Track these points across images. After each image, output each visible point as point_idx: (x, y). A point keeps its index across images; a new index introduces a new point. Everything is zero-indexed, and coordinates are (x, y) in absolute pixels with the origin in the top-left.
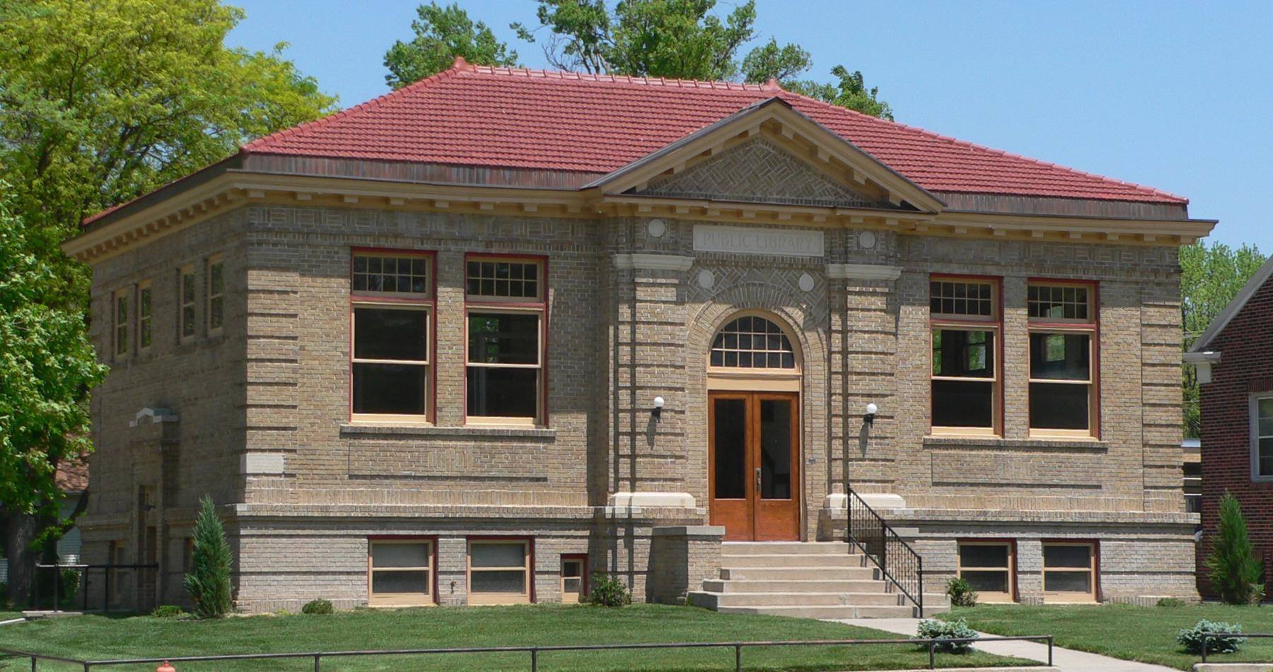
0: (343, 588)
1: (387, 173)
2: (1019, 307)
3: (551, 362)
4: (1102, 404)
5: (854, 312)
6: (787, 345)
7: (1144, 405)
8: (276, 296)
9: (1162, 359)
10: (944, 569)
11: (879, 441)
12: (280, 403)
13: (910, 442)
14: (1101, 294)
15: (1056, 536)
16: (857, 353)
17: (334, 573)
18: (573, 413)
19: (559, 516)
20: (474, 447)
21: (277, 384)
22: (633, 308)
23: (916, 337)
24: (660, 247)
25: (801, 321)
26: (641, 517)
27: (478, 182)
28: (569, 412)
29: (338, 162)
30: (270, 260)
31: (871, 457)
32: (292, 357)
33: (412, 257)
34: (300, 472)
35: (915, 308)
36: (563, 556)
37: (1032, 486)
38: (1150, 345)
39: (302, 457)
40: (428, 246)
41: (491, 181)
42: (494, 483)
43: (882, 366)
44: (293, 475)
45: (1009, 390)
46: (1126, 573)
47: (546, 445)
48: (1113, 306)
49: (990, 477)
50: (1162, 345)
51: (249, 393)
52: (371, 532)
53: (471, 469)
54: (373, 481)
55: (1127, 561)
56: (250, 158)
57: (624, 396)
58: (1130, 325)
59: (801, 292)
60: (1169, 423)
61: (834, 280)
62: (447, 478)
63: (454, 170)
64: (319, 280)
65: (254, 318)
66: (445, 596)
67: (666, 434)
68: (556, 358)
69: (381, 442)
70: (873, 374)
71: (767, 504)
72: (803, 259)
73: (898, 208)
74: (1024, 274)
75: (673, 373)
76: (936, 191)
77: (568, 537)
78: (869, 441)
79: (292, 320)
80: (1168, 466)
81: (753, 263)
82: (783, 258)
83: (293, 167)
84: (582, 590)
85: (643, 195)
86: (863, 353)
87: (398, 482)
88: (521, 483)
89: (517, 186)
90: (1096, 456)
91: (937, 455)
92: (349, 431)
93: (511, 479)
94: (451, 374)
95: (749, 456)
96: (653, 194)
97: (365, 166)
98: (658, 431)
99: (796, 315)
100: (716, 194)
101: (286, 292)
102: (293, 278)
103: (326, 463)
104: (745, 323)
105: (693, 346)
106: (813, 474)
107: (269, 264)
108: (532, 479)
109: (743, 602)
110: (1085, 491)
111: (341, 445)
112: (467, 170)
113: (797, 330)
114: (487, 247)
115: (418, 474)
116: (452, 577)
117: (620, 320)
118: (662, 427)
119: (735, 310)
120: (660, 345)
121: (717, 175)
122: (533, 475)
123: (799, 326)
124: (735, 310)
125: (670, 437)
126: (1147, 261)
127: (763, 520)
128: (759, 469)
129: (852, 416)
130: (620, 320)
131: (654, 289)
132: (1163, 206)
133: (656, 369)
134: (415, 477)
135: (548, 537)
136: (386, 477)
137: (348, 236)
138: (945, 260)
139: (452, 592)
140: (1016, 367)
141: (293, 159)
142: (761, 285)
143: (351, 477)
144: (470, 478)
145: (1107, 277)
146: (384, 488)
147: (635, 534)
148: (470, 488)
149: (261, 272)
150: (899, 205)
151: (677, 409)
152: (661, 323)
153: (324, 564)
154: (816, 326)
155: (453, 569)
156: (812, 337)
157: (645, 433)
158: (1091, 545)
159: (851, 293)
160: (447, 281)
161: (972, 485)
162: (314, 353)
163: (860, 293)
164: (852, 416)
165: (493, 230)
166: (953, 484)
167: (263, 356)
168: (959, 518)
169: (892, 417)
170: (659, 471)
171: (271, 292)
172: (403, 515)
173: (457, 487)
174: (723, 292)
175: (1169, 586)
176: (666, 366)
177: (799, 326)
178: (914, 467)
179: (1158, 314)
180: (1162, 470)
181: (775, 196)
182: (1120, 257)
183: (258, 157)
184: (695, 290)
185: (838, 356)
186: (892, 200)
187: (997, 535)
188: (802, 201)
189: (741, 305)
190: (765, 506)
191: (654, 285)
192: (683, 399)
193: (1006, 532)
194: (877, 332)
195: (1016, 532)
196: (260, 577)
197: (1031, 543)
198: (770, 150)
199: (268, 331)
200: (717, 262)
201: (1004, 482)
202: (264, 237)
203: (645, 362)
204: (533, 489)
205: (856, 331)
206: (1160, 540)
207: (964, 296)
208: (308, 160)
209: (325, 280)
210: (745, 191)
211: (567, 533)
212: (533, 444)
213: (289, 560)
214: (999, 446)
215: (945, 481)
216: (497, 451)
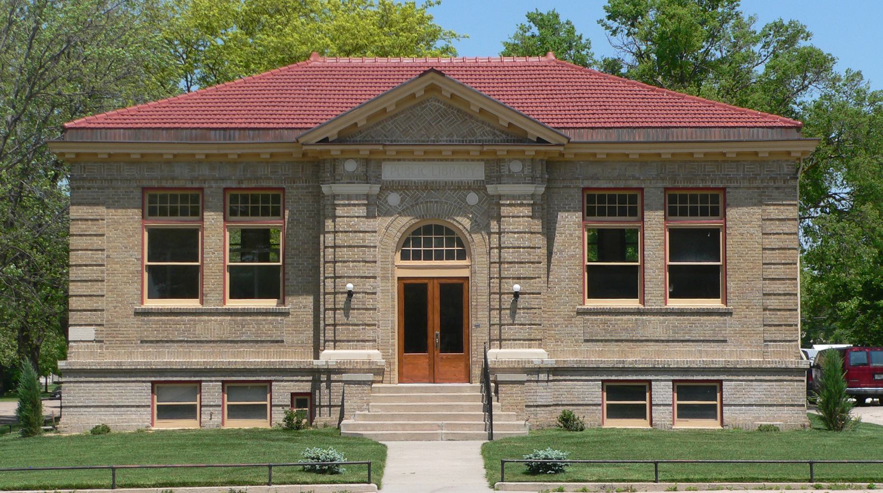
0: (134, 417)
1: (164, 137)
2: (657, 209)
3: (288, 261)
4: (728, 279)
5: (506, 219)
6: (460, 244)
7: (764, 279)
8: (90, 222)
9: (781, 245)
10: (591, 402)
11: (526, 311)
12: (92, 294)
13: (566, 310)
14: (727, 197)
15: (684, 378)
16: (509, 248)
17: (128, 406)
18: (303, 295)
19: (287, 367)
20: (230, 320)
21: (91, 281)
22: (499, 222)
23: (571, 235)
24: (352, 179)
25: (468, 226)
26: (336, 367)
27: (230, 139)
28: (300, 295)
29: (130, 131)
30: (85, 199)
31: (520, 322)
32: (100, 263)
33: (271, 193)
34: (107, 339)
35: (569, 213)
36: (293, 395)
37: (668, 341)
38: (770, 234)
39: (108, 329)
40: (196, 185)
41: (239, 138)
42: (245, 344)
43: (528, 257)
44: (102, 341)
45: (649, 271)
46: (745, 405)
47: (283, 318)
48: (737, 206)
49: (631, 335)
50: (781, 234)
51: (70, 287)
52: (153, 379)
53: (227, 336)
54: (158, 344)
55: (747, 396)
56: (69, 131)
57: (329, 283)
58: (753, 220)
59: (469, 205)
60: (786, 292)
61: (493, 196)
62: (211, 342)
63: (213, 132)
64: (119, 211)
65: (75, 238)
66: (206, 422)
67: (358, 309)
68: (291, 258)
69: (164, 318)
70: (522, 263)
71: (444, 357)
72: (468, 183)
73: (533, 142)
74: (660, 185)
75: (364, 266)
76: (559, 128)
77: (296, 381)
78: (518, 311)
79: (101, 238)
80: (785, 325)
81: (428, 187)
82: (452, 182)
83: (99, 137)
84: (309, 418)
85: (334, 142)
86: (514, 248)
87: (176, 345)
88: (265, 344)
89: (258, 141)
90: (722, 318)
91: (588, 320)
92: (140, 311)
93: (257, 342)
94: (213, 271)
95: (430, 323)
96: (350, 141)
97: (150, 132)
98: (352, 307)
99: (465, 222)
100: (399, 139)
101: (97, 220)
102: (101, 210)
103: (125, 332)
104: (428, 229)
105: (384, 247)
106: (477, 336)
107: (85, 201)
108: (272, 342)
109: (361, 429)
110: (712, 344)
111: (134, 320)
112: (222, 132)
113: (466, 233)
114: (239, 183)
115: (189, 339)
116: (211, 409)
117: (326, 230)
118: (355, 303)
119: (417, 220)
120: (354, 247)
121: (400, 126)
122: (272, 339)
123: (467, 230)
124: (417, 220)
125: (362, 311)
126: (767, 171)
127: (442, 368)
128: (438, 332)
129: (504, 293)
130: (326, 230)
131: (349, 208)
132: (779, 130)
133: (351, 264)
134: (187, 342)
135: (282, 381)
136: (167, 342)
137: (139, 180)
138: (595, 178)
139: (211, 419)
140: (655, 254)
141: (99, 131)
142: (436, 202)
143: (142, 342)
144: (227, 342)
145: (732, 185)
146: (166, 349)
147: (332, 379)
148: (226, 348)
149: (79, 207)
150: (535, 140)
151: (368, 291)
152: (355, 232)
153: (120, 400)
154: (481, 229)
155: (212, 403)
156: (477, 237)
157: (343, 309)
158: (647, 384)
159: (504, 205)
160: (211, 208)
161: (617, 341)
162: (116, 260)
163: (510, 205)
164: (504, 293)
165: (244, 171)
166: (602, 341)
167: (80, 262)
168: (601, 366)
169: (539, 294)
170: (353, 335)
171: (87, 220)
172: (174, 367)
173: (218, 348)
174: (407, 208)
175: (783, 415)
176: (359, 262)
177: (467, 230)
178: (569, 329)
179: (777, 211)
180: (780, 328)
181: (445, 138)
182: (744, 169)
183: (74, 131)
184: (386, 208)
185: (496, 251)
186: (529, 137)
187: (635, 378)
188: (466, 141)
189: (422, 217)
190: (442, 358)
191: (349, 205)
192: (374, 284)
193: (642, 375)
194: (525, 233)
195: (651, 375)
196: (76, 409)
197: (663, 383)
198: (441, 106)
199: (84, 246)
200: (402, 187)
201: (644, 338)
202: (81, 183)
203: (343, 259)
204: (274, 348)
205: (508, 233)
206: (776, 381)
207: (248, 207)
208: (109, 131)
209: (124, 210)
210: (422, 136)
211: (295, 378)
212: (273, 318)
213: (96, 398)
214: (639, 312)
215: (594, 338)
216: (246, 322)
